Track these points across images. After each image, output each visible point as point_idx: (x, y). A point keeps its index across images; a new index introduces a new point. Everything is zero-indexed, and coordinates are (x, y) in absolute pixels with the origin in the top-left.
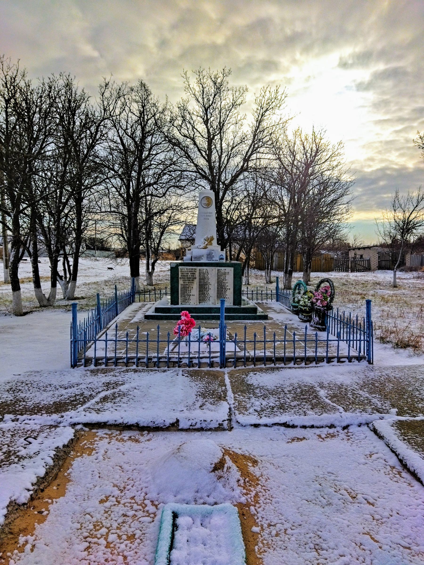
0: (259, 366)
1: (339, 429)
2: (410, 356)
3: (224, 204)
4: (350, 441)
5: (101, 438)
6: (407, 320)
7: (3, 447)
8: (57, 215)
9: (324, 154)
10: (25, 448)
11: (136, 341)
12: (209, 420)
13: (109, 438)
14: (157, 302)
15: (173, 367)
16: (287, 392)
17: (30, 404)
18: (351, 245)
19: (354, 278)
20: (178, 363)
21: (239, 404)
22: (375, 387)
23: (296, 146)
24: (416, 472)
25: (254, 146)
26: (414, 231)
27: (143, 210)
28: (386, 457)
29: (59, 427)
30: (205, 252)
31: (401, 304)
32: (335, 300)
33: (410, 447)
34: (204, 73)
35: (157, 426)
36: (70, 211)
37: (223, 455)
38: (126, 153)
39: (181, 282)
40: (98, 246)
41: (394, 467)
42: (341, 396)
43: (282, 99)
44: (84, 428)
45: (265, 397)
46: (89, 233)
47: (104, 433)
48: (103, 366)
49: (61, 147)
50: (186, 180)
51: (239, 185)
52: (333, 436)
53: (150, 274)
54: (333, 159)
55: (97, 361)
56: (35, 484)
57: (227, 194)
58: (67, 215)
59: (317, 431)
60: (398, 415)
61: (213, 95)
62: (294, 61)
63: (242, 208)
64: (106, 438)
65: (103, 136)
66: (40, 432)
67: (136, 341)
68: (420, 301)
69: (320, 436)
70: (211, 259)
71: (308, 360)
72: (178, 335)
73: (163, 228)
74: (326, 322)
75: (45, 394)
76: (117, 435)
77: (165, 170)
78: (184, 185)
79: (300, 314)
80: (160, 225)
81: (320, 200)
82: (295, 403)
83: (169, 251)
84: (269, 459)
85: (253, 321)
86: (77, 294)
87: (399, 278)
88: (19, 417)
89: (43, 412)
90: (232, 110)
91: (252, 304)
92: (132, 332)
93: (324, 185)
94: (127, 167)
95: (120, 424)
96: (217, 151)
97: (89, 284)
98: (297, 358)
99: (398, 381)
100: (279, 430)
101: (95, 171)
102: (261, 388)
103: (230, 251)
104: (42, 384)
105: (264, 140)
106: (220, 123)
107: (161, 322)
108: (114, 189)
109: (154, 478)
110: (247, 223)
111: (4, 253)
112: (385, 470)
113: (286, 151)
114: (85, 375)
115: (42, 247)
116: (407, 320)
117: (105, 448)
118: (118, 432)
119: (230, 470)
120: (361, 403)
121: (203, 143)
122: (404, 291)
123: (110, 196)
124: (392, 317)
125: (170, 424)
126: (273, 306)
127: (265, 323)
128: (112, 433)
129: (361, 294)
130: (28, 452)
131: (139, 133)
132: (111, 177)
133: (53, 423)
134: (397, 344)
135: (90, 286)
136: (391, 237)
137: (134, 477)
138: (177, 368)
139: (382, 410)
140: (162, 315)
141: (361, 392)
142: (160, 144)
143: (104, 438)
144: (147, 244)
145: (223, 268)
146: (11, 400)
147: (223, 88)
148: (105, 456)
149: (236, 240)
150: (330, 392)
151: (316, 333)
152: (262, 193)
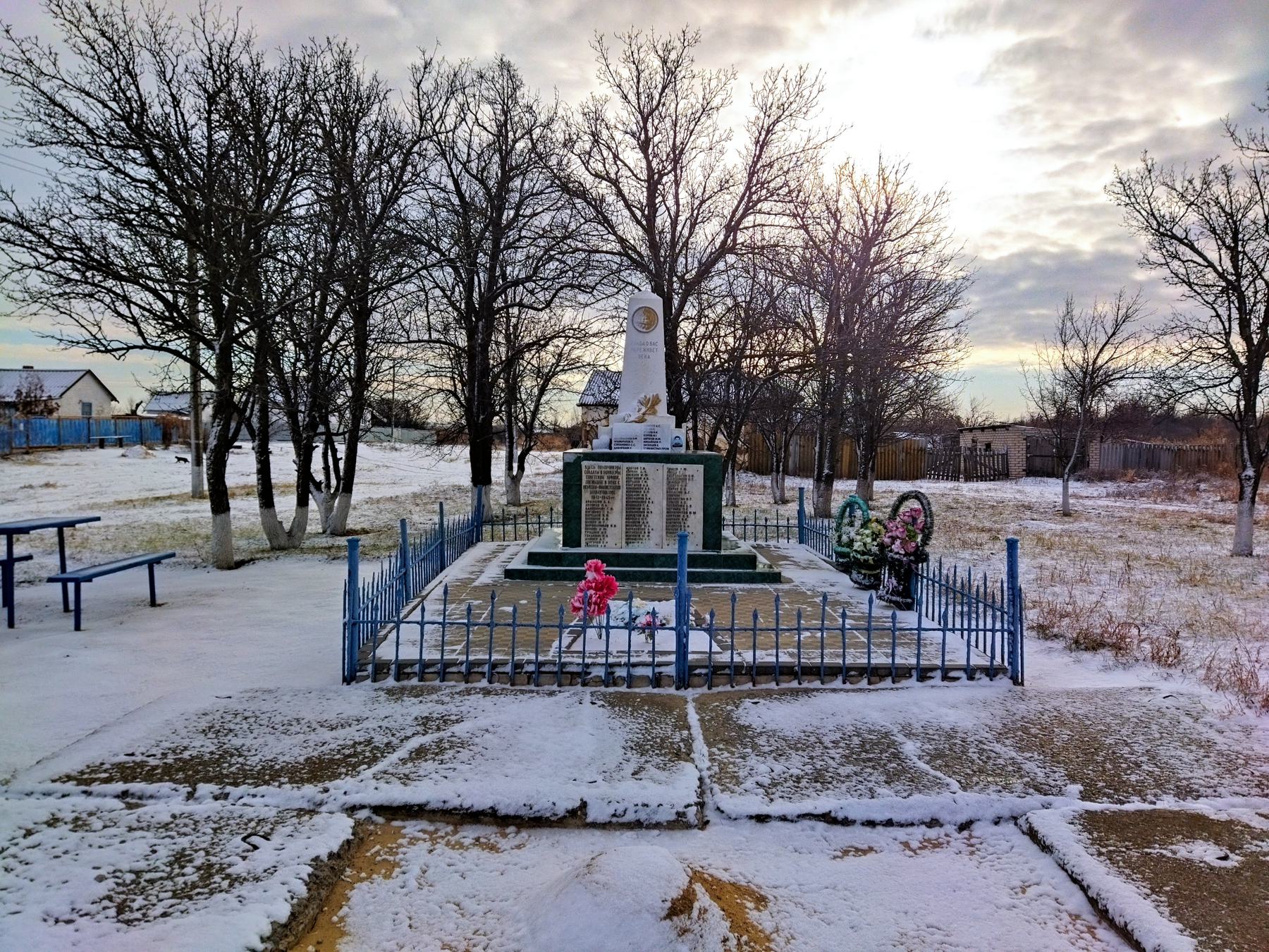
0: (764, 686)
1: (950, 829)
2: (1106, 668)
3: (682, 325)
4: (975, 857)
5: (413, 841)
6: (1097, 589)
7: (195, 855)
8: (312, 346)
9: (905, 217)
10: (244, 858)
11: (488, 625)
12: (654, 804)
13: (431, 839)
14: (533, 541)
15: (571, 684)
16: (830, 745)
17: (253, 761)
18: (963, 421)
19: (972, 494)
20: (581, 677)
21: (721, 769)
22: (1033, 736)
23: (841, 198)
24: (1129, 928)
25: (750, 197)
26: (1108, 390)
27: (501, 339)
28: (1060, 893)
29: (317, 813)
30: (640, 429)
31: (1081, 554)
32: (933, 542)
33: (1114, 870)
34: (642, 40)
35: (538, 815)
36: (342, 339)
37: (690, 882)
38: (466, 212)
39: (586, 496)
40: (400, 419)
41: (1077, 917)
42: (954, 756)
43: (813, 95)
44: (375, 818)
45: (779, 754)
46: (383, 387)
47: (419, 828)
48: (414, 681)
49: (327, 199)
50: (597, 272)
51: (716, 283)
52: (937, 845)
53: (515, 480)
54: (925, 228)
55: (402, 670)
56: (268, 938)
57: (688, 303)
58: (334, 348)
59: (901, 833)
60: (1083, 798)
61: (660, 86)
62: (819, 28)
63: (722, 334)
64: (424, 840)
65: (418, 175)
66: (277, 823)
67: (488, 625)
68: (1125, 547)
69: (906, 845)
70: (654, 446)
71: (874, 674)
72: (581, 613)
73: (546, 378)
74: (913, 588)
75: (287, 741)
76: (447, 834)
77: (551, 248)
78: (592, 284)
79: (854, 572)
80: (538, 372)
81: (895, 318)
82: (849, 769)
83: (557, 431)
84: (793, 894)
85: (747, 586)
86: (351, 523)
87: (1075, 496)
88: (229, 789)
89: (282, 780)
90: (703, 120)
91: (745, 547)
92: (478, 607)
93: (908, 286)
94: (469, 245)
95: (455, 809)
96: (668, 209)
97: (378, 501)
98: (849, 669)
99: (1081, 724)
100: (813, 829)
101: (398, 253)
102: (772, 734)
103: (695, 429)
104: (279, 719)
105: (772, 185)
106: (674, 147)
107: (541, 584)
108: (438, 292)
109: (533, 932)
110: (732, 371)
111: (193, 431)
112: (1057, 922)
113: (818, 208)
114: (375, 700)
115: (278, 417)
116: (1097, 589)
117: (422, 861)
118: (450, 828)
119: (705, 916)
120: (1000, 772)
121: (638, 193)
122: (1086, 524)
123: (430, 307)
124: (1063, 582)
125: (568, 812)
126: (790, 553)
127: (776, 590)
128: (437, 831)
129: (990, 530)
130: (250, 867)
131: (495, 169)
132: (434, 265)
133: (305, 806)
134: (1076, 642)
135: (381, 506)
136: (1055, 403)
137: (488, 928)
138: (579, 687)
139: (1047, 787)
140: (545, 568)
141: (998, 747)
142: (542, 193)
143: (418, 839)
144: (509, 415)
145: (679, 466)
146: (212, 753)
147: (683, 73)
148: (422, 881)
149: (707, 406)
150: (927, 746)
151: (894, 614)
152: (766, 302)
